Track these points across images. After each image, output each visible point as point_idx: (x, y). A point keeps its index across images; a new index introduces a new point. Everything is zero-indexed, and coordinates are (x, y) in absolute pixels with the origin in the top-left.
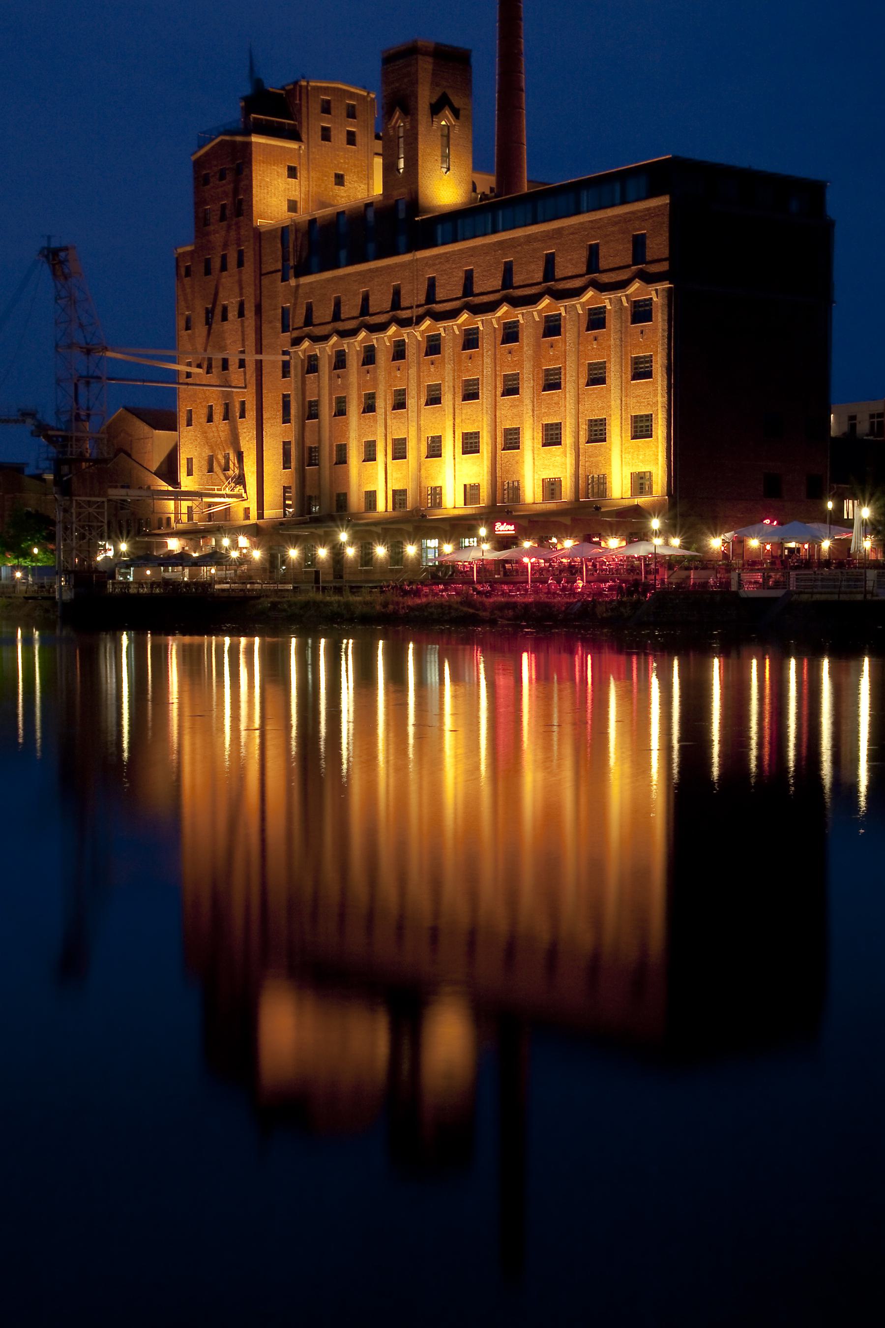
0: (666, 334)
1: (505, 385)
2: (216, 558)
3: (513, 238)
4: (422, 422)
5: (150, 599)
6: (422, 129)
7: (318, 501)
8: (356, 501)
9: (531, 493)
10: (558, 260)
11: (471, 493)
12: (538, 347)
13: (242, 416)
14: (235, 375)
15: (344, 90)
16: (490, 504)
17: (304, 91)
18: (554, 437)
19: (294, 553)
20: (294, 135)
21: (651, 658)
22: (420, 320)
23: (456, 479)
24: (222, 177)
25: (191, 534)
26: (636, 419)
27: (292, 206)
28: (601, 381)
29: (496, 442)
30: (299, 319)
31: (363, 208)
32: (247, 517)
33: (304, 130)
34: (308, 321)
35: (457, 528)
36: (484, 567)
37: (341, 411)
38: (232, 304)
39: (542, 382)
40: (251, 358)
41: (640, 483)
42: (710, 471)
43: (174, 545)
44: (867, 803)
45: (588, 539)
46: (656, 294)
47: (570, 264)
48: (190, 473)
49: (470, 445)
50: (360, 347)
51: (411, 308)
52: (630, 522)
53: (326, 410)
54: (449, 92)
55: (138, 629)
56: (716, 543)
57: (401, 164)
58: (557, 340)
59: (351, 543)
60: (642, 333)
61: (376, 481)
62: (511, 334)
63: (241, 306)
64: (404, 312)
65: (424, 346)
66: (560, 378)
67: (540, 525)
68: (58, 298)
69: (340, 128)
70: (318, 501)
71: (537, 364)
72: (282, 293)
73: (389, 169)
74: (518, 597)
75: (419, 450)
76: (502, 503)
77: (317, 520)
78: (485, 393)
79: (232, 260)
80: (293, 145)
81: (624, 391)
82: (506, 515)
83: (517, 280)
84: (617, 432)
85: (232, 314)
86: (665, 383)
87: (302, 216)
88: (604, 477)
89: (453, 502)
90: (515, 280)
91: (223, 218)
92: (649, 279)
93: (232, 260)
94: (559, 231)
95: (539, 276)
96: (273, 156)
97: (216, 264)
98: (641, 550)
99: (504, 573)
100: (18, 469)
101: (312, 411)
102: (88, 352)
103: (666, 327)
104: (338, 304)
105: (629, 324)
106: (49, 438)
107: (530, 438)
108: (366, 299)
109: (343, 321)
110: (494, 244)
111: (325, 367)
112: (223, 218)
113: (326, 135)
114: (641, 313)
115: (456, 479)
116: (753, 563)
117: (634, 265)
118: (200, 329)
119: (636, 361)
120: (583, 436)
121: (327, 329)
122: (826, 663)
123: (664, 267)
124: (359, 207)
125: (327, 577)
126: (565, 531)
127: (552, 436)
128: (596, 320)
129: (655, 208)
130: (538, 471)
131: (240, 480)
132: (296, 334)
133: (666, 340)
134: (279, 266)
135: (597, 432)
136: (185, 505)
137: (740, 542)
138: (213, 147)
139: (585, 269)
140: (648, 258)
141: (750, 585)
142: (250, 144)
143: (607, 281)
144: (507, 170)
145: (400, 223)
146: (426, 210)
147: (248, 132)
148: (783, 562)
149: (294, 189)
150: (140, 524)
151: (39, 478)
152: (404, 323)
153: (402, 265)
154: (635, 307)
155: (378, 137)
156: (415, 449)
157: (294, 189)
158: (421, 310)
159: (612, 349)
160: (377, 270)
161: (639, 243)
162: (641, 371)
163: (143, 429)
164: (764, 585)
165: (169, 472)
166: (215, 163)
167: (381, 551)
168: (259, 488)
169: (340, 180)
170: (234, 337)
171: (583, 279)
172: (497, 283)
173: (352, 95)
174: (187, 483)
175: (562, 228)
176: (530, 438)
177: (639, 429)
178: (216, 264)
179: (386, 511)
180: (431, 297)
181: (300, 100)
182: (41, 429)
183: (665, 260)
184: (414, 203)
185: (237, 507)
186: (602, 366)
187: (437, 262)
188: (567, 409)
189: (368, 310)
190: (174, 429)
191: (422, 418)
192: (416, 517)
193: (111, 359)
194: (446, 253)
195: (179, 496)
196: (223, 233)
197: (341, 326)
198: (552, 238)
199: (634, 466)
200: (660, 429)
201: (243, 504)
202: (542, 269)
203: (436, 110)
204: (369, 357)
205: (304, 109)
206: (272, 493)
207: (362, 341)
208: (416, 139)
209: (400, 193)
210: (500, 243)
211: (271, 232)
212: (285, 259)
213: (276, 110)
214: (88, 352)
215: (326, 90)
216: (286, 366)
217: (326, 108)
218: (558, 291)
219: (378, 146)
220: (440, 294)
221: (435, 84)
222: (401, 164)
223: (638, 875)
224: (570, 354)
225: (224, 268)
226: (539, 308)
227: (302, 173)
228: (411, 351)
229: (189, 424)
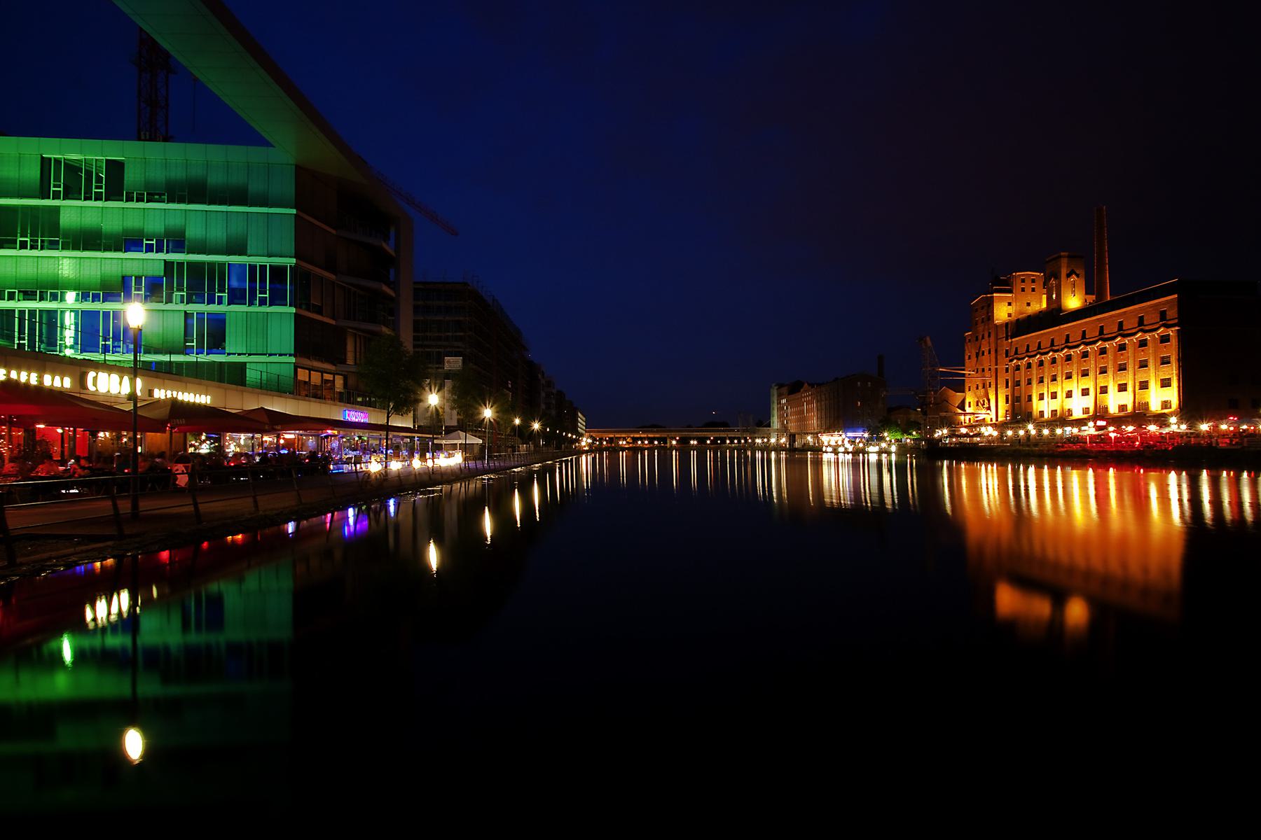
2: (979, 435)
5: (954, 448)
7: (1020, 412)
8: (1035, 413)
9: (1113, 410)
14: (987, 373)
19: (1010, 433)
20: (1010, 291)
21: (846, 499)
23: (1078, 406)
25: (970, 427)
26: (1162, 380)
27: (1010, 315)
35: (1080, 423)
36: (1091, 437)
37: (1029, 382)
38: (986, 349)
40: (993, 368)
41: (1166, 404)
43: (964, 431)
44: (182, 402)
45: (1140, 426)
46: (1172, 332)
47: (1130, 324)
52: (1161, 419)
53: (1023, 383)
55: (950, 459)
56: (1204, 427)
57: (15, 578)
61: (1043, 406)
67: (1117, 421)
70: (1020, 412)
71: (1115, 360)
72: (1005, 345)
73: (1049, 299)
74: (1107, 448)
76: (1100, 413)
77: (1018, 422)
82: (1102, 419)
87: (1013, 318)
89: (1077, 414)
96: (1001, 299)
98: (1165, 431)
99: (1101, 439)
101: (1018, 384)
111: (1023, 369)
114: (1165, 339)
116: (1224, 435)
118: (974, 358)
126: (1127, 424)
130: (1115, 401)
131: (989, 408)
136: (967, 418)
137: (1216, 427)
141: (1223, 444)
144: (1100, 295)
145: (1056, 315)
148: (1237, 434)
149: (1011, 309)
150: (951, 423)
156: (1061, 395)
157: (1011, 309)
161: (1163, 315)
163: (951, 392)
164: (1230, 444)
167: (1046, 432)
168: (1000, 408)
169: (1029, 304)
170: (987, 361)
174: (968, 410)
180: (1067, 341)
184: (1059, 308)
185: (988, 419)
192: (1061, 419)
199: (1162, 395)
200: (1175, 383)
201: (990, 416)
203: (1069, 276)
204: (1041, 363)
206: (1001, 412)
209: (1054, 306)
211: (1001, 325)
217: (1023, 281)
222: (15, 578)
228: (1059, 361)
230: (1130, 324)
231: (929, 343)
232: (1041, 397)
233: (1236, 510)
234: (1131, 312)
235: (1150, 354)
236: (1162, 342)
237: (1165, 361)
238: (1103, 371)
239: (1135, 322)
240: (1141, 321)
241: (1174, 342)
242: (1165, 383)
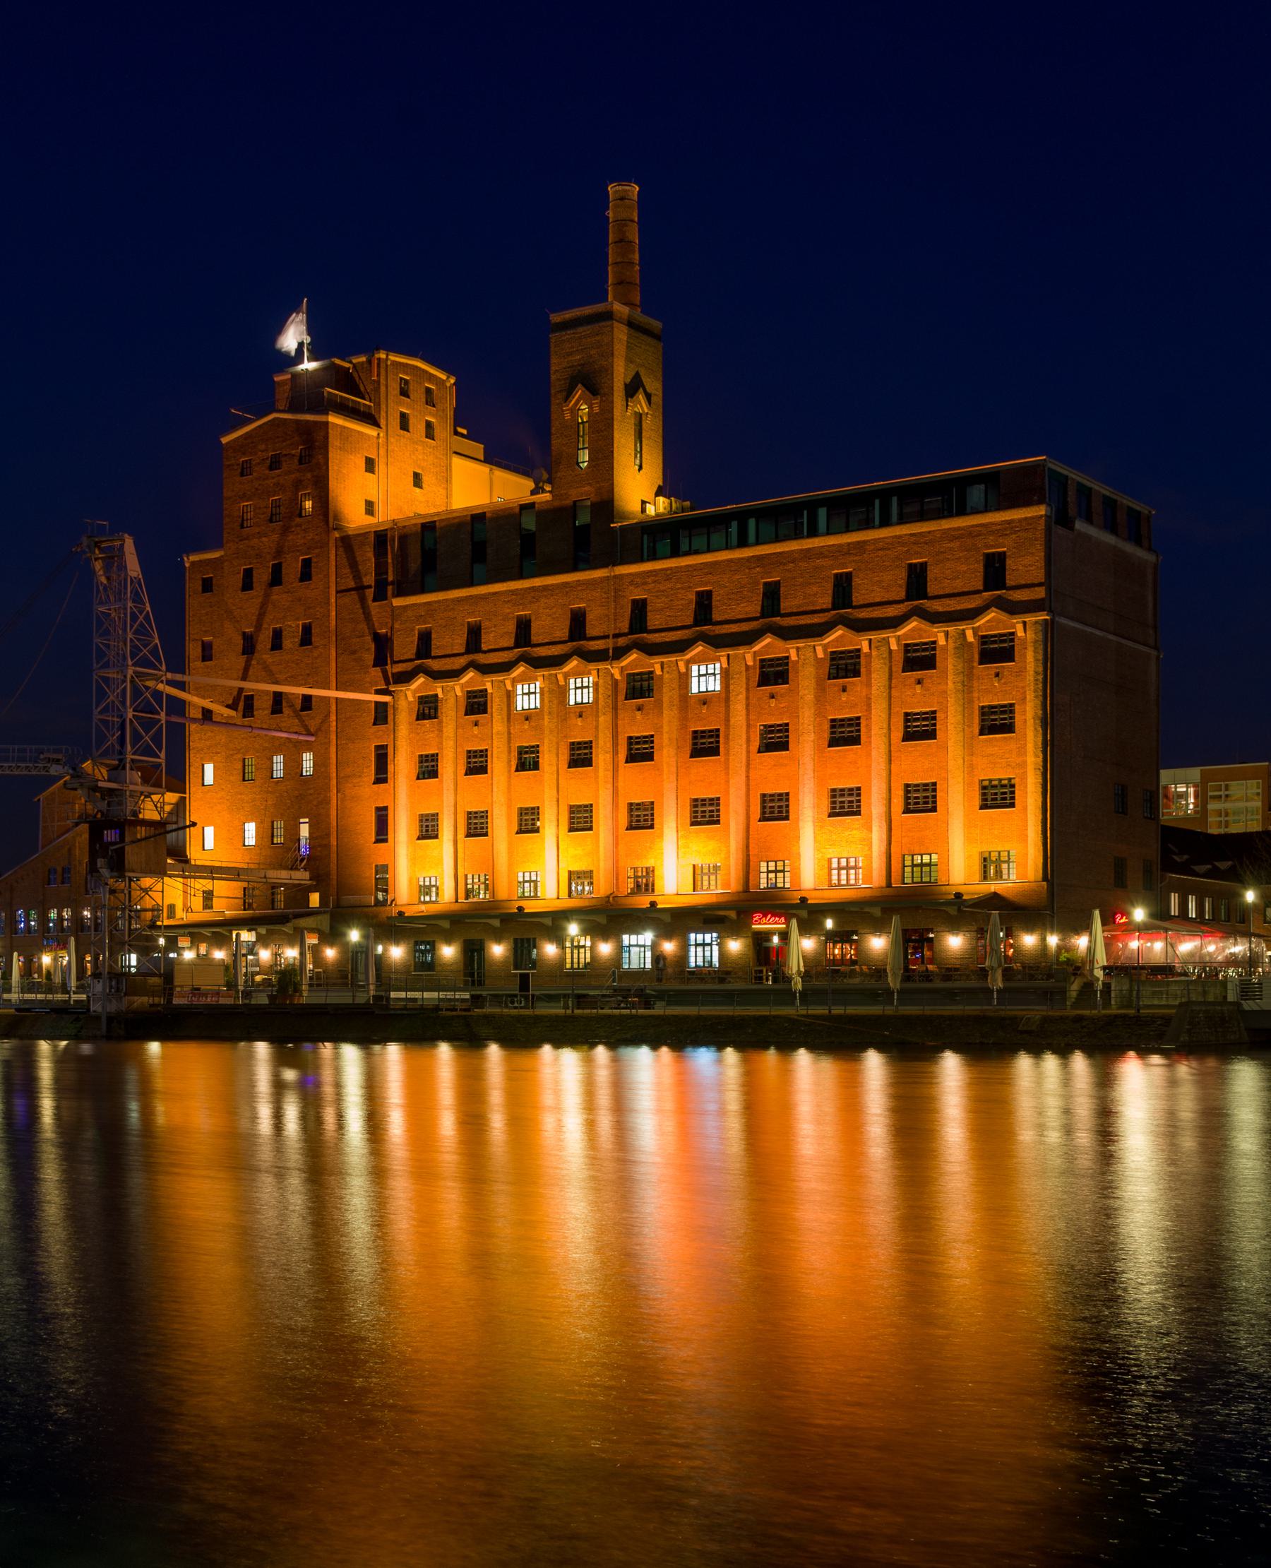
0: (1040, 677)
1: (630, 749)
3: (780, 553)
4: (620, 784)
6: (617, 412)
10: (856, 581)
12: (820, 689)
15: (423, 370)
16: (740, 888)
17: (383, 365)
18: (1008, 796)
23: (547, 869)
26: (573, 810)
28: (535, 766)
29: (617, 821)
31: (517, 510)
33: (383, 414)
39: (826, 736)
47: (879, 586)
50: (755, 661)
51: (606, 637)
54: (642, 373)
57: (585, 456)
58: (853, 683)
60: (997, 675)
64: (592, 643)
65: (623, 687)
66: (859, 731)
71: (819, 713)
75: (615, 820)
78: (602, 757)
80: (371, 431)
86: (1040, 739)
90: (782, 605)
92: (1014, 609)
94: (860, 546)
95: (825, 600)
103: (1040, 669)
105: (975, 664)
109: (485, 652)
110: (748, 559)
114: (997, 651)
117: (986, 590)
124: (512, 508)
127: (845, 804)
129: (1020, 520)
133: (1040, 686)
138: (260, 427)
139: (903, 594)
140: (1009, 582)
142: (327, 423)
143: (941, 609)
146: (624, 516)
154: (983, 643)
158: (461, 661)
160: (545, 588)
161: (995, 571)
166: (263, 447)
171: (901, 606)
173: (431, 378)
175: (864, 542)
177: (989, 797)
179: (889, 885)
181: (378, 375)
183: (1040, 585)
186: (535, 750)
187: (650, 580)
189: (1004, 583)
191: (620, 778)
194: (666, 569)
196: (275, 537)
198: (848, 553)
199: (989, 845)
202: (830, 592)
205: (383, 388)
207: (416, 691)
208: (610, 426)
210: (759, 558)
218: (781, 628)
220: (487, 641)
221: (629, 360)
222: (585, 456)
226: (624, 664)
227: (381, 467)
230: (879, 586)
231: (133, 567)
232: (428, 829)
233: (733, 1211)
234: (885, 545)
235: (950, 695)
236: (765, 680)
237: (997, 722)
238: (920, 729)
239: (971, 574)
240: (917, 581)
241: (1030, 659)
242: (997, 796)
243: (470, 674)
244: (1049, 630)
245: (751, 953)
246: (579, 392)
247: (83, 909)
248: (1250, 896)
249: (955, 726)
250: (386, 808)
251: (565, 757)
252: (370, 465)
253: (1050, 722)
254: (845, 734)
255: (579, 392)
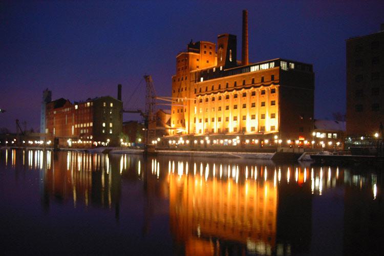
11: (235, 129)
12: (250, 98)
13: (185, 111)
22: (225, 91)
24: (183, 61)
28: (264, 105)
30: (198, 91)
32: (200, 132)
34: (200, 92)
41: (273, 128)
42: (288, 126)
46: (276, 87)
48: (174, 123)
49: (235, 119)
52: (270, 136)
59: (156, 140)
62: (227, 97)
63: (186, 88)
68: (147, 86)
69: (208, 51)
71: (250, 101)
79: (184, 78)
81: (269, 108)
83: (246, 84)
84: (268, 116)
85: (184, 90)
88: (264, 127)
91: (182, 69)
92: (275, 84)
93: (184, 78)
97: (181, 79)
100: (137, 122)
102: (153, 98)
104: (207, 88)
106: (144, 116)
107: (248, 117)
108: (213, 87)
112: (182, 69)
113: (205, 52)
114: (273, 91)
115: (232, 126)
119: (272, 102)
120: (260, 117)
121: (204, 93)
122: (330, 170)
123: (278, 81)
125: (91, 146)
127: (253, 117)
128: (254, 94)
130: (216, 126)
132: (198, 94)
134: (194, 79)
135: (263, 117)
142: (189, 55)
147: (189, 52)
150: (162, 133)
151: (140, 124)
152: (221, 92)
153: (222, 80)
155: (216, 53)
159: (266, 99)
162: (273, 103)
165: (169, 123)
172: (242, 84)
174: (173, 126)
176: (248, 117)
178: (181, 79)
180: (235, 85)
182: (142, 114)
188: (257, 111)
190: (170, 114)
193: (158, 100)
195: (171, 129)
197: (220, 90)
199: (272, 123)
212: (196, 78)
213: (196, 48)
214: (153, 98)
215: (205, 43)
216: (195, 101)
217: (205, 47)
219: (216, 55)
220: (229, 86)
223: (271, 213)
224: (257, 100)
225: (182, 80)
228: (222, 98)
229: (174, 113)
243: (262, 87)
244: (279, 88)
245: (54, 143)
246: (221, 48)
247: (108, 138)
248: (376, 135)
249: (268, 104)
250: (264, 115)
251: (270, 104)
252: (198, 60)
253: (279, 104)
254: (253, 105)
255: (221, 48)
